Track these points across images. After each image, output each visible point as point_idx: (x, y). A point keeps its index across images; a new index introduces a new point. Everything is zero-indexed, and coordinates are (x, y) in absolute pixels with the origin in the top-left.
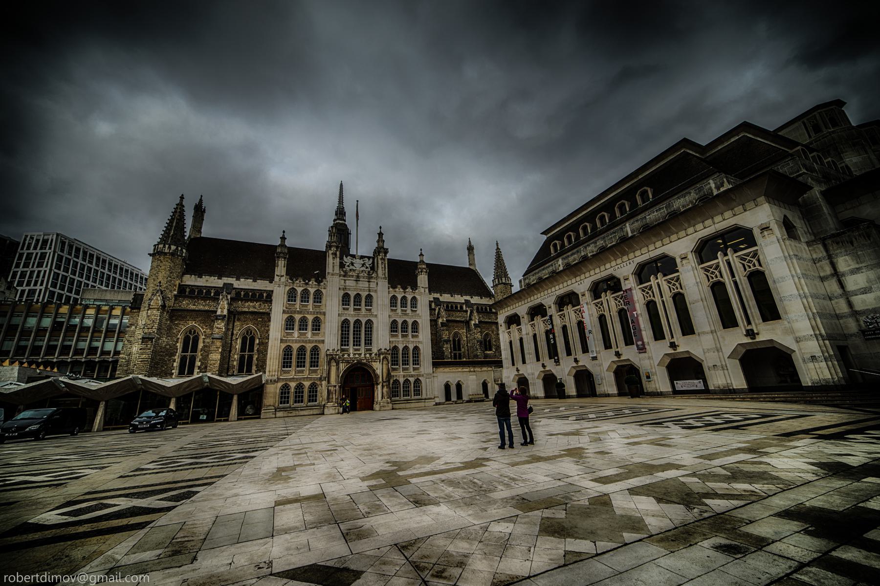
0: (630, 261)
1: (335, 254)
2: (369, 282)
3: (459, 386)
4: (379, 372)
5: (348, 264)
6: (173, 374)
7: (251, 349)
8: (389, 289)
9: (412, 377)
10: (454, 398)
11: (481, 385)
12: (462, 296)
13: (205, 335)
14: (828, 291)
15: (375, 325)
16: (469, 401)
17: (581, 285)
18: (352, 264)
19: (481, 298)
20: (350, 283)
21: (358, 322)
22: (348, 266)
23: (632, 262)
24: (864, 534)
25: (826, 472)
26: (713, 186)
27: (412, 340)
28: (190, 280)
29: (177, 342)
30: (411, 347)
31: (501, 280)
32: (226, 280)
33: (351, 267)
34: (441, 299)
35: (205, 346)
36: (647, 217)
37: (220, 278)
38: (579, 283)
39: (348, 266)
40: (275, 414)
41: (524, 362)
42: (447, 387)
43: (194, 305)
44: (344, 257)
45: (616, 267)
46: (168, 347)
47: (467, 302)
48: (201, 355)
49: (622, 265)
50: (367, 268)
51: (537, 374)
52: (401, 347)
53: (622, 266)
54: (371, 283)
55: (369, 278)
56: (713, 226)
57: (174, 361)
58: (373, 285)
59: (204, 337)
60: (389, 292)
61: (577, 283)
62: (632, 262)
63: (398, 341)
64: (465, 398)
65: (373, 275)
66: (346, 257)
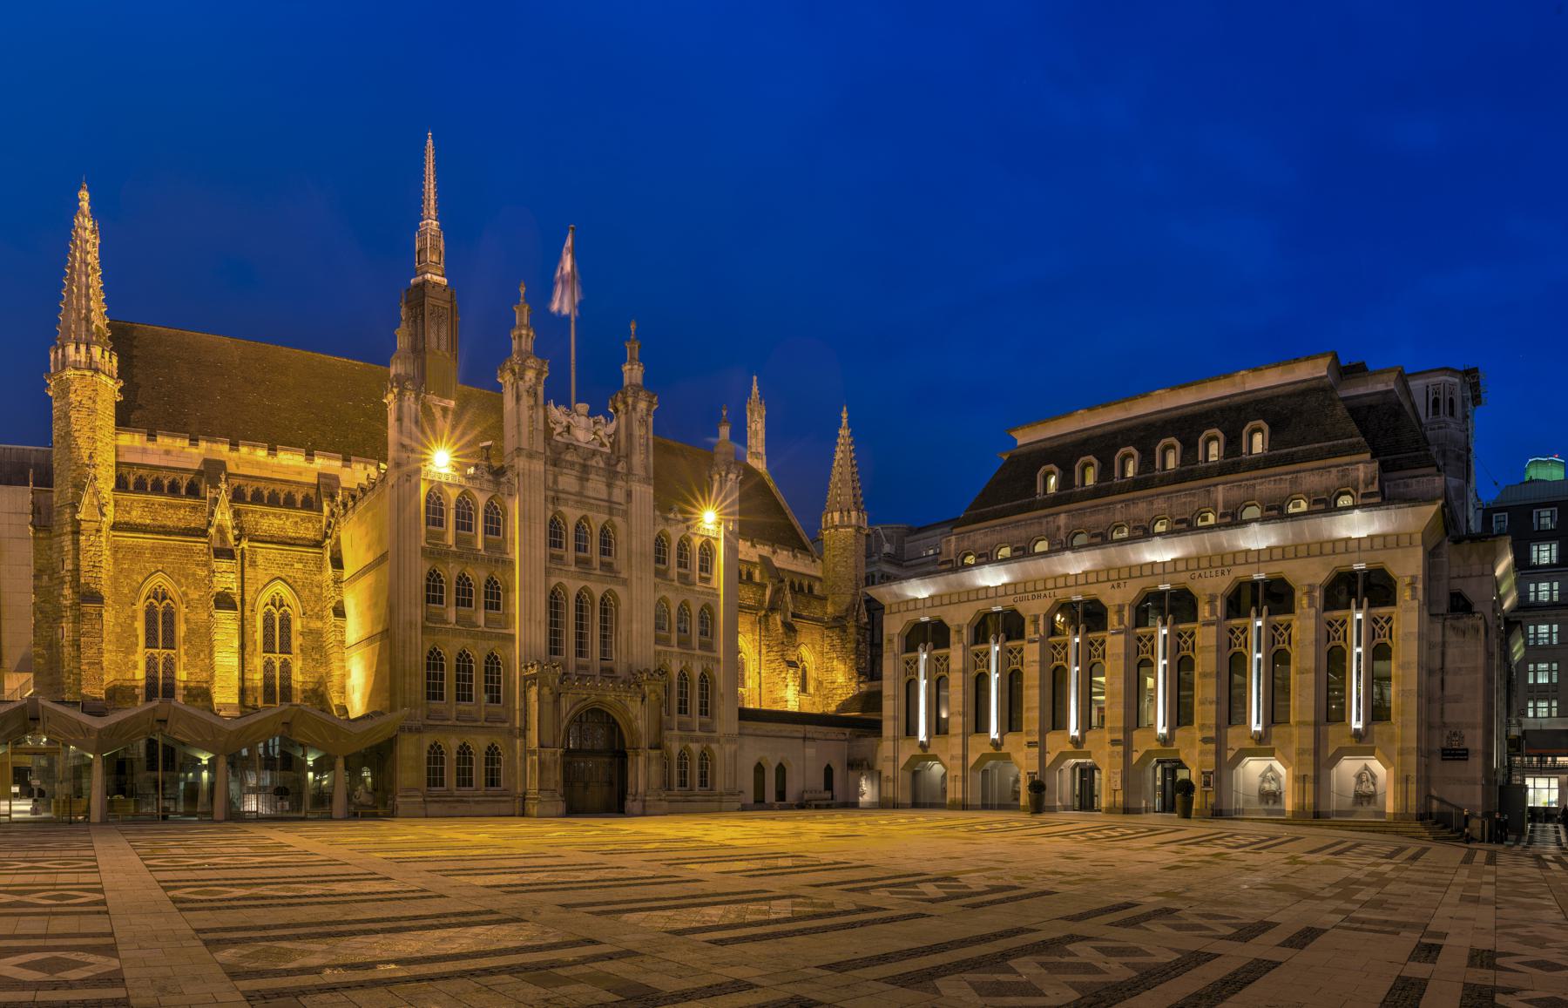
0: (1225, 569)
3: (781, 770)
4: (641, 725)
6: (137, 697)
9: (697, 741)
10: (770, 795)
12: (753, 546)
14: (1439, 627)
15: (623, 607)
17: (1117, 590)
19: (795, 556)
23: (1226, 573)
26: (1362, 475)
27: (698, 652)
29: (134, 618)
30: (696, 671)
31: (849, 517)
32: (322, 463)
36: (1257, 488)
38: (1115, 583)
39: (560, 434)
40: (425, 808)
45: (1197, 573)
47: (765, 562)
48: (186, 654)
49: (1208, 571)
52: (675, 669)
53: (1208, 574)
56: (1357, 554)
61: (1110, 584)
62: (1226, 573)
63: (671, 653)
64: (791, 796)
65: (619, 468)
66: (556, 406)
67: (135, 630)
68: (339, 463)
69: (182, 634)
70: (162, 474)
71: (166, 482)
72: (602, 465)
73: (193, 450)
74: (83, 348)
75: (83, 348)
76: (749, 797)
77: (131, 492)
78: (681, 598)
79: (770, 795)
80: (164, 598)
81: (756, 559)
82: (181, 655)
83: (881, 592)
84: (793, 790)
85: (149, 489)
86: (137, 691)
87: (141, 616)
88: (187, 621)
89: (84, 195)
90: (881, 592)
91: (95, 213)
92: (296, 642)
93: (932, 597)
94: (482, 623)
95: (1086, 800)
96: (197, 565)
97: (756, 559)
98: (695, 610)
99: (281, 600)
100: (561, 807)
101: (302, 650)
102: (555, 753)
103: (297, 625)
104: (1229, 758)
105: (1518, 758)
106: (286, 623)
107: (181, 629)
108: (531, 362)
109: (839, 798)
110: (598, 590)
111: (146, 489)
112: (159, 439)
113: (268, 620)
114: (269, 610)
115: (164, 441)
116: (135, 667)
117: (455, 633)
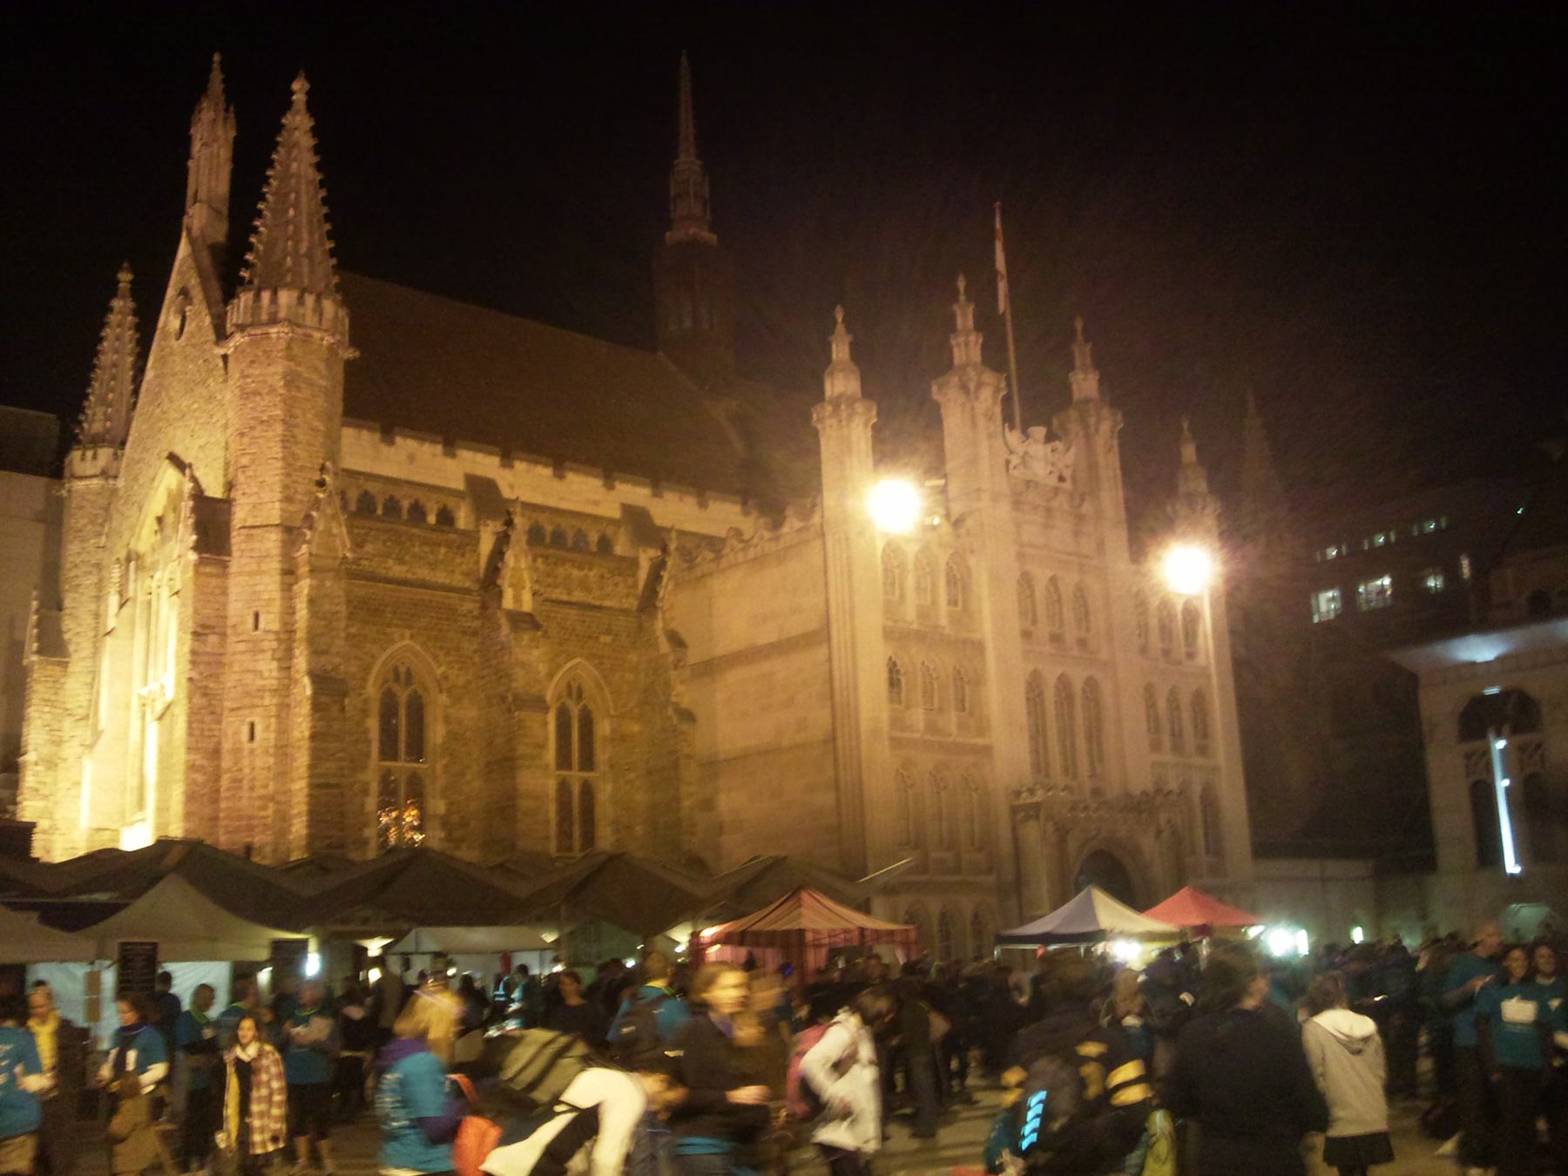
7: (588, 762)
12: (610, 486)
13: (449, 691)
21: (1064, 683)
35: (452, 736)
43: (401, 561)
59: (444, 699)
67: (366, 731)
68: (495, 460)
69: (439, 740)
72: (1066, 506)
77: (379, 519)
78: (1058, 671)
81: (460, 485)
83: (1419, 657)
85: (380, 512)
87: (375, 708)
88: (447, 720)
89: (299, 88)
90: (1419, 657)
91: (312, 107)
92: (602, 755)
93: (1499, 659)
94: (953, 728)
96: (464, 633)
97: (460, 485)
98: (1185, 699)
99: (409, 673)
101: (612, 766)
103: (603, 728)
104: (510, 1010)
107: (437, 733)
109: (1321, 1062)
110: (1078, 678)
111: (543, 539)
112: (399, 440)
114: (563, 704)
115: (406, 444)
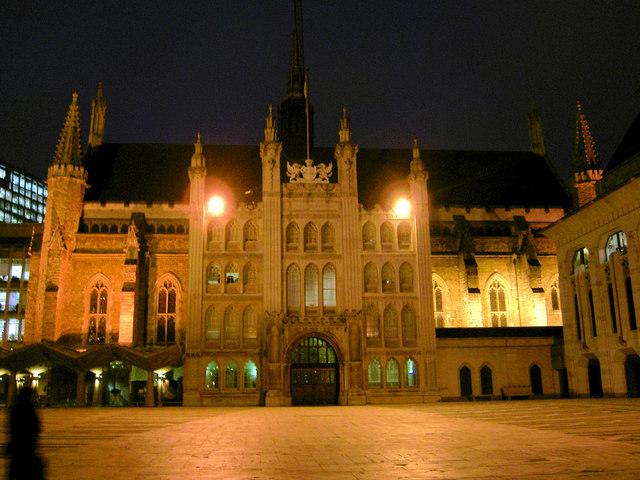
1: (274, 161)
2: (308, 202)
3: (486, 373)
5: (293, 176)
8: (360, 211)
10: (477, 390)
11: (528, 372)
16: (504, 398)
18: (301, 176)
20: (297, 204)
22: (295, 179)
24: (156, 369)
25: (97, 330)
28: (93, 209)
33: (299, 180)
34: (469, 217)
37: (127, 204)
39: (295, 179)
41: (633, 326)
42: (465, 373)
44: (288, 165)
46: (73, 304)
50: (324, 179)
51: (613, 353)
54: (331, 204)
55: (329, 194)
57: (82, 324)
58: (334, 206)
60: (360, 216)
64: (497, 392)
66: (291, 165)
70: (107, 223)
71: (110, 226)
73: (126, 209)
74: (62, 166)
75: (62, 166)
76: (456, 391)
79: (477, 390)
80: (102, 286)
82: (108, 316)
84: (499, 382)
86: (82, 337)
88: (113, 298)
92: (178, 306)
95: (596, 390)
100: (290, 400)
102: (280, 367)
103: (178, 297)
105: (18, 384)
106: (172, 296)
108: (273, 146)
113: (162, 296)
115: (110, 206)
116: (82, 324)
117: (223, 298)
